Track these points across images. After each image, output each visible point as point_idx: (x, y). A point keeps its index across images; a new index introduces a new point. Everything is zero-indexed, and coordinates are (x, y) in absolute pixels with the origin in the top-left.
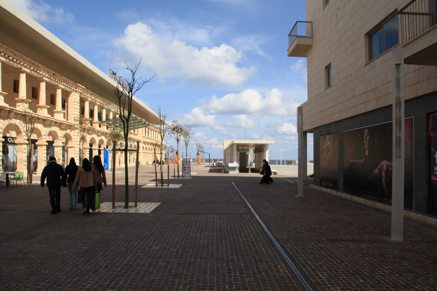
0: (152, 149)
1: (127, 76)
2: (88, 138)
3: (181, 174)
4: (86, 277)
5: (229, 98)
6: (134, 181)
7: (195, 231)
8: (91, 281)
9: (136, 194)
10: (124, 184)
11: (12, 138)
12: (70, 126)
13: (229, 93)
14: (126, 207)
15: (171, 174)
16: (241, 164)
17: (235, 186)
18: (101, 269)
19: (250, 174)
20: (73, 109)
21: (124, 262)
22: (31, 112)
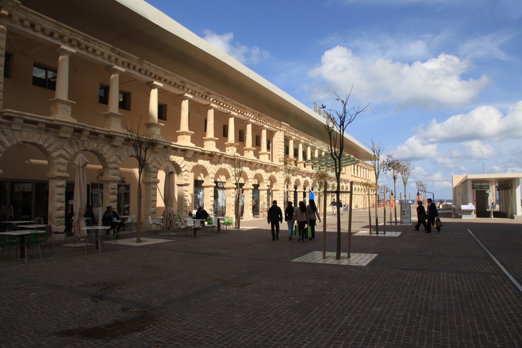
0: (361, 190)
1: (337, 109)
2: (293, 179)
3: (399, 219)
4: (301, 335)
5: (455, 121)
6: (347, 229)
7: (426, 292)
8: (307, 340)
9: (349, 243)
10: (336, 231)
11: (222, 182)
12: (275, 167)
13: (456, 114)
14: (338, 257)
15: (388, 220)
16: (477, 207)
17: (473, 235)
18: (317, 328)
19: (492, 220)
20: (278, 150)
21: (341, 322)
22: (239, 155)
